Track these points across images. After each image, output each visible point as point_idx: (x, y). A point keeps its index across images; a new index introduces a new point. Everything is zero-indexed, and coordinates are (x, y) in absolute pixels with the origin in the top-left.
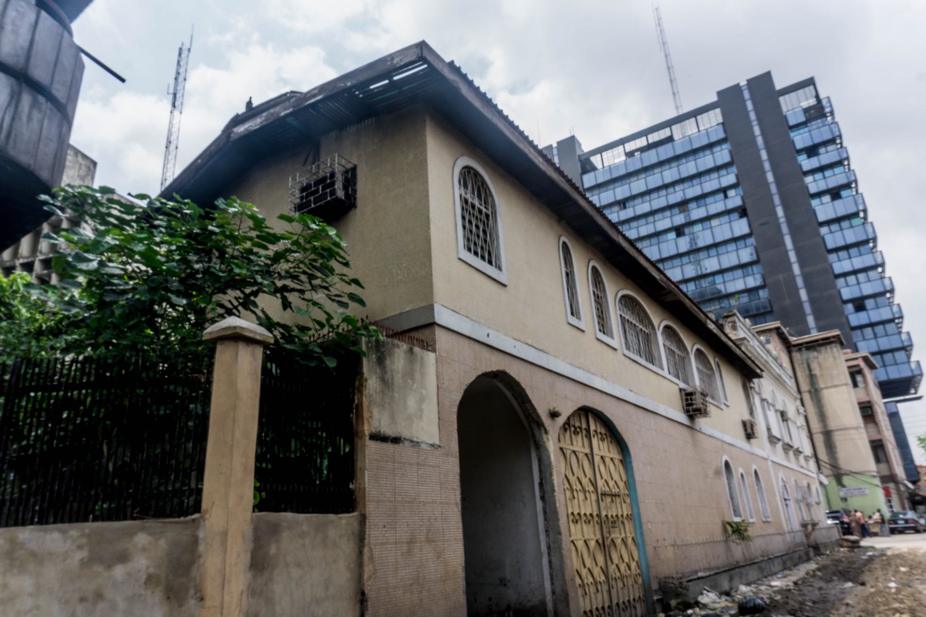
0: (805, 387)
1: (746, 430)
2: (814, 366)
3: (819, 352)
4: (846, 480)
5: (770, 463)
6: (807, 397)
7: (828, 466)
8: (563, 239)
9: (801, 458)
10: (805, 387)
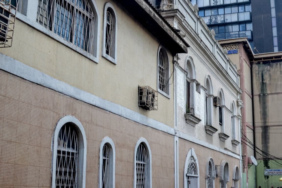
0: (257, 91)
1: (140, 98)
2: (266, 77)
3: (271, 66)
4: (270, 163)
5: (176, 139)
6: (256, 99)
7: (261, 153)
8: (109, 5)
9: (228, 142)
10: (257, 91)
